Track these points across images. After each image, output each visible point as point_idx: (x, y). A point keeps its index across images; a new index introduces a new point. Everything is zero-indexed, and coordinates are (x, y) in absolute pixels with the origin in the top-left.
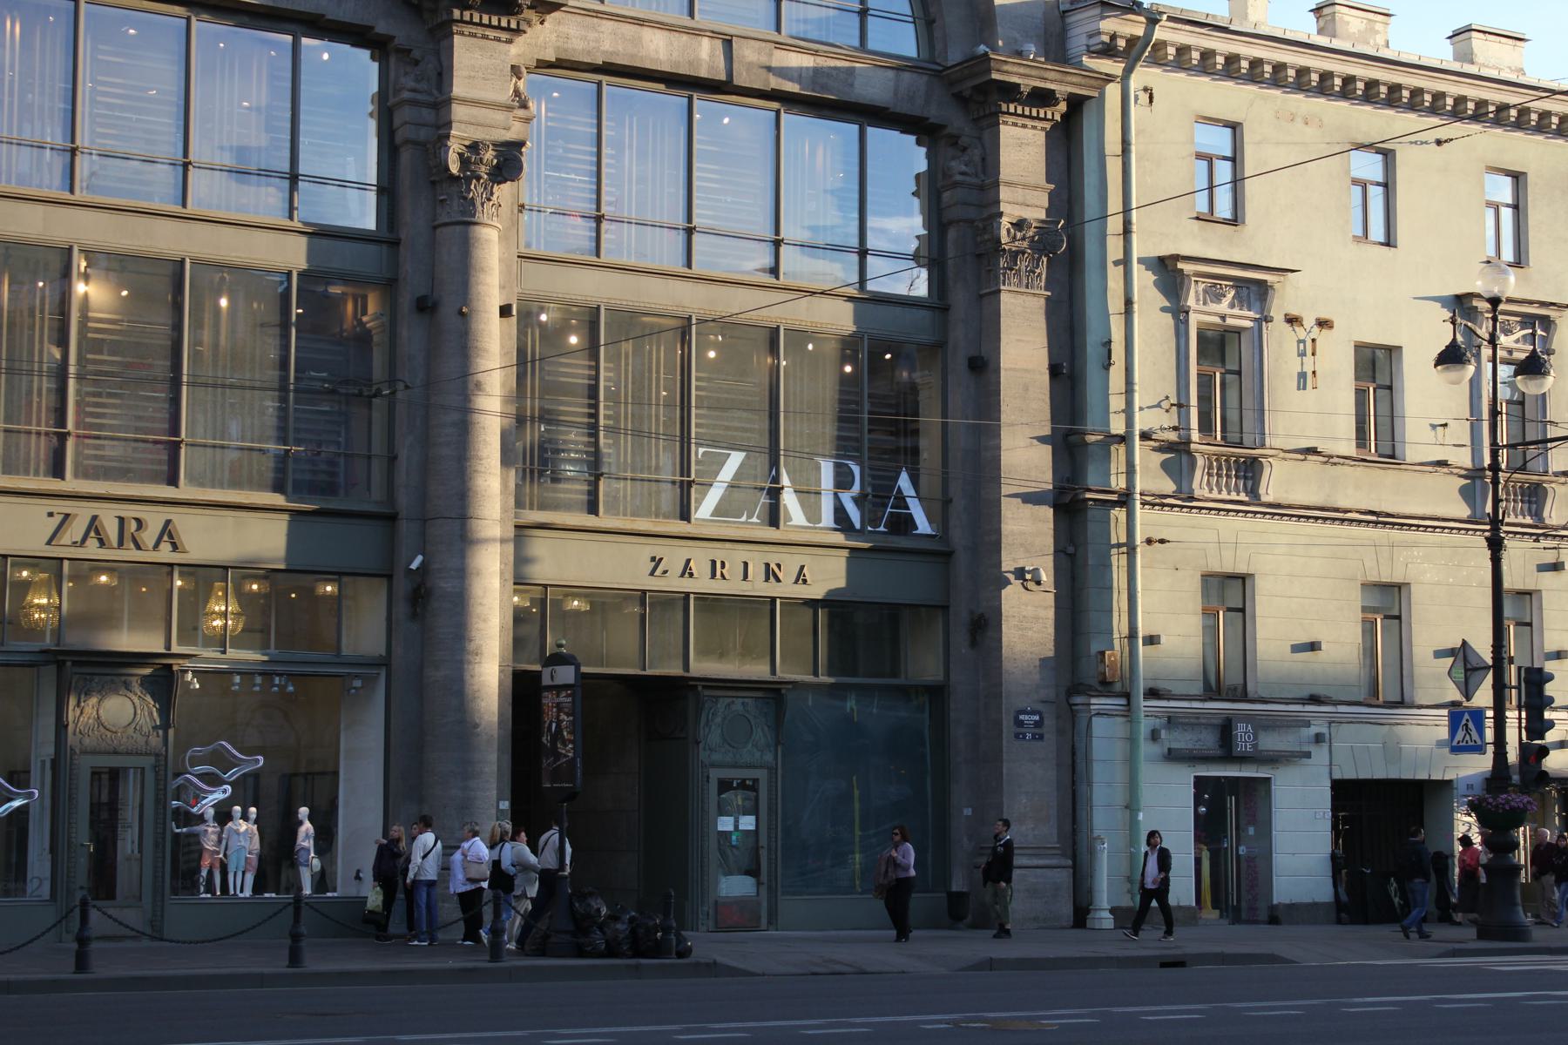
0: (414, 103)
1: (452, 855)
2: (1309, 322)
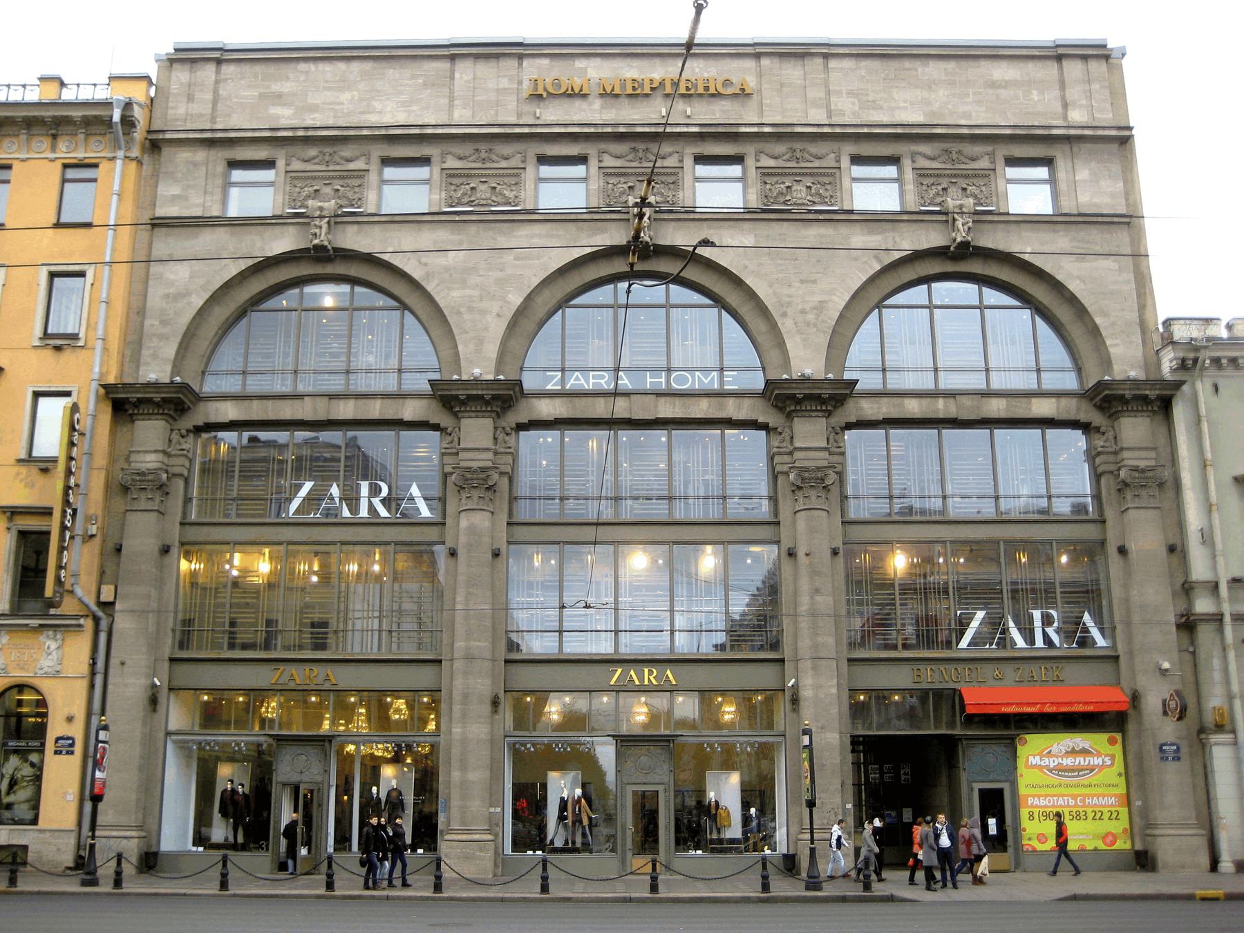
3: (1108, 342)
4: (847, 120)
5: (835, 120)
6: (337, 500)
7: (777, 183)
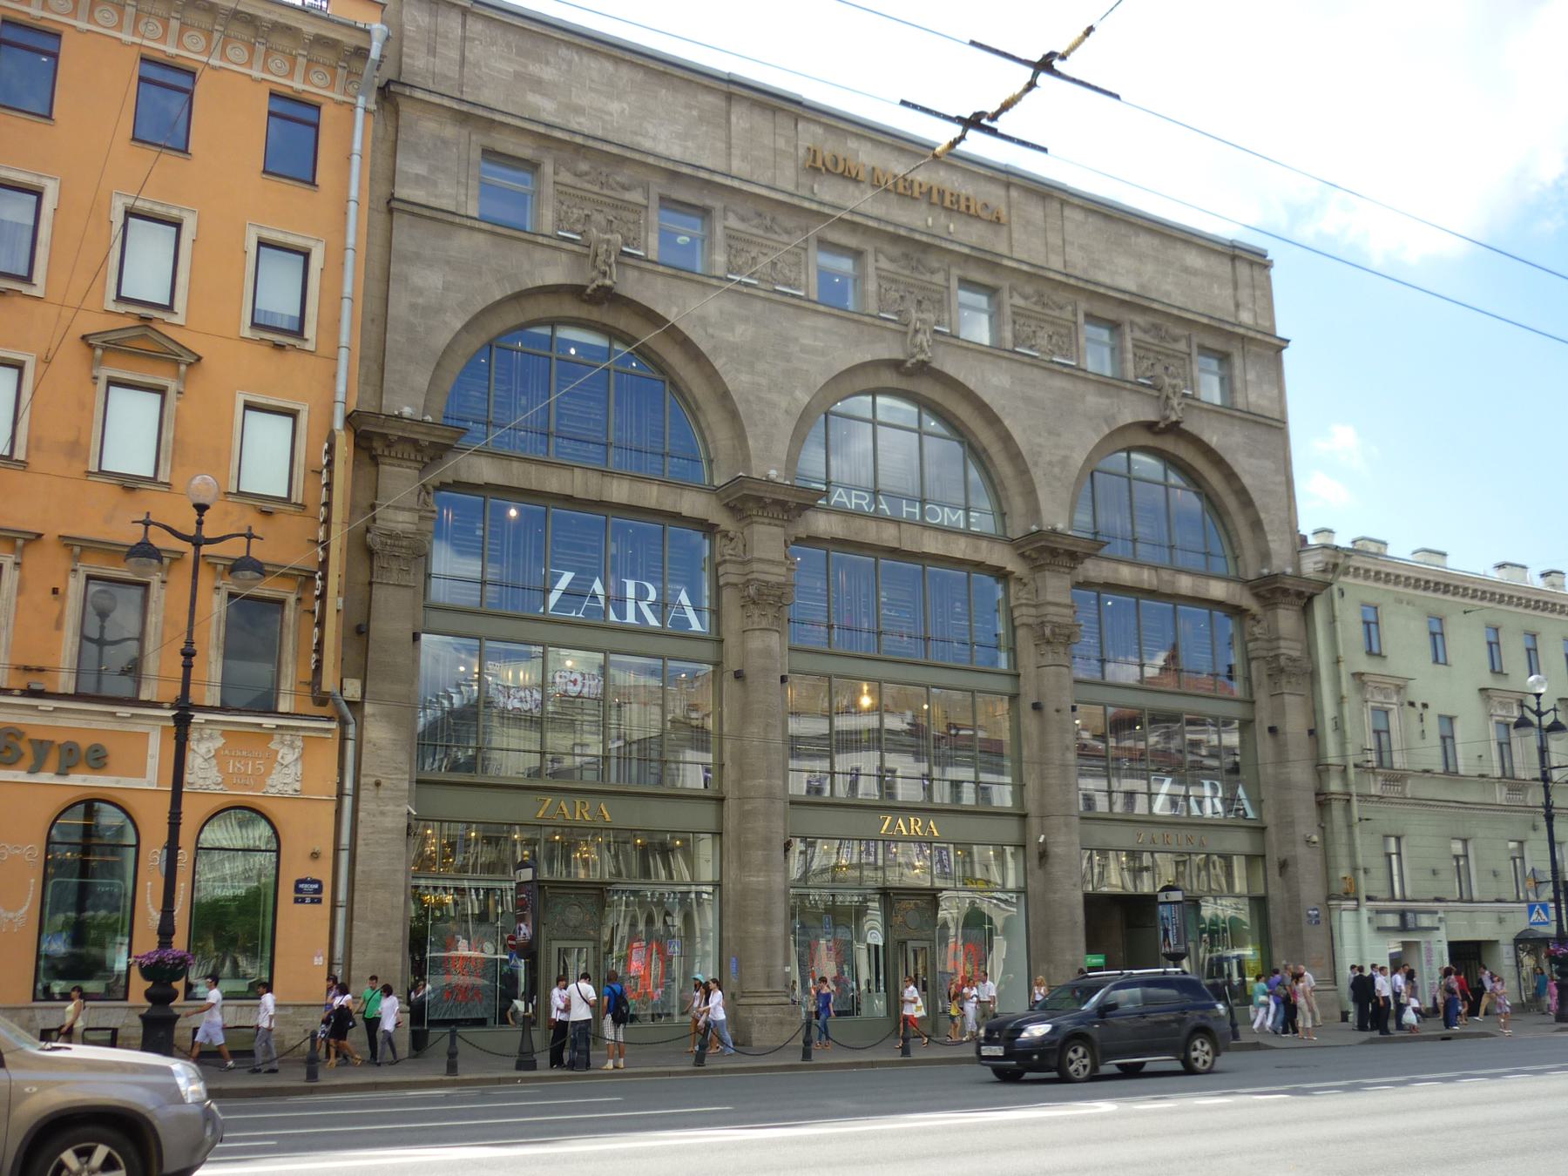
0: (1027, 605)
1: (916, 986)
2: (1418, 705)
3: (1270, 538)
4: (1077, 273)
5: (1069, 271)
6: (602, 599)
7: (575, 206)
